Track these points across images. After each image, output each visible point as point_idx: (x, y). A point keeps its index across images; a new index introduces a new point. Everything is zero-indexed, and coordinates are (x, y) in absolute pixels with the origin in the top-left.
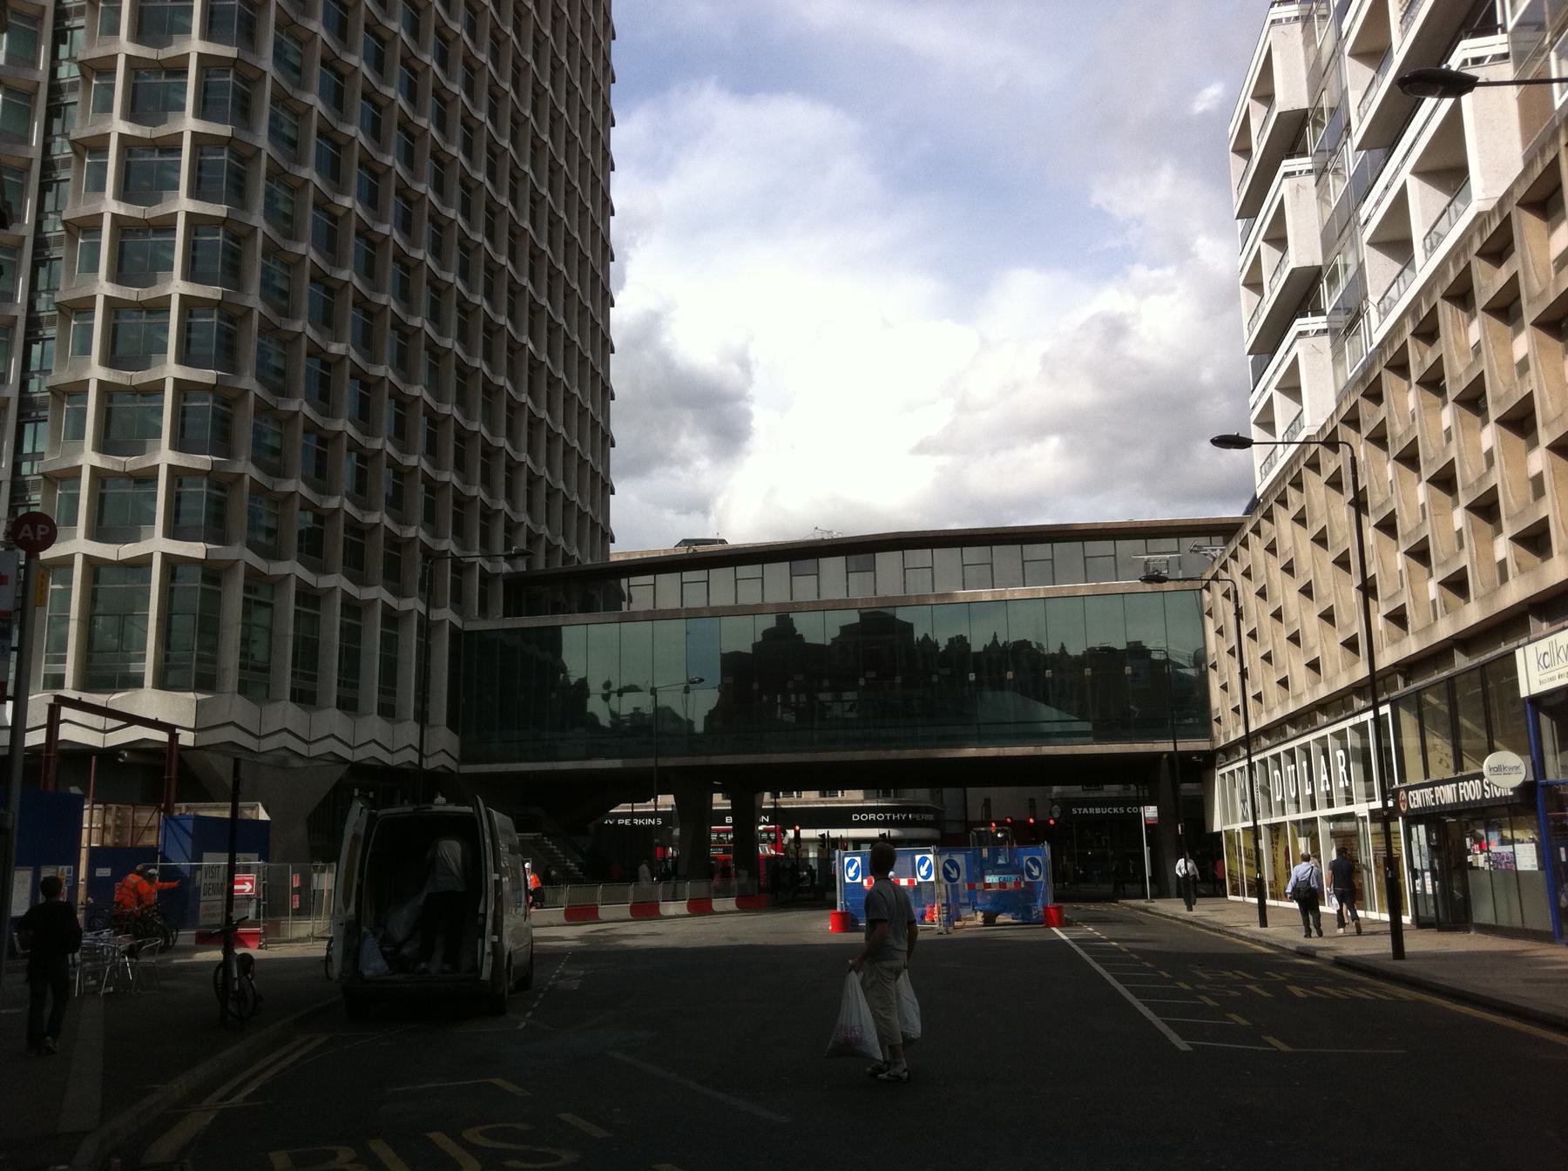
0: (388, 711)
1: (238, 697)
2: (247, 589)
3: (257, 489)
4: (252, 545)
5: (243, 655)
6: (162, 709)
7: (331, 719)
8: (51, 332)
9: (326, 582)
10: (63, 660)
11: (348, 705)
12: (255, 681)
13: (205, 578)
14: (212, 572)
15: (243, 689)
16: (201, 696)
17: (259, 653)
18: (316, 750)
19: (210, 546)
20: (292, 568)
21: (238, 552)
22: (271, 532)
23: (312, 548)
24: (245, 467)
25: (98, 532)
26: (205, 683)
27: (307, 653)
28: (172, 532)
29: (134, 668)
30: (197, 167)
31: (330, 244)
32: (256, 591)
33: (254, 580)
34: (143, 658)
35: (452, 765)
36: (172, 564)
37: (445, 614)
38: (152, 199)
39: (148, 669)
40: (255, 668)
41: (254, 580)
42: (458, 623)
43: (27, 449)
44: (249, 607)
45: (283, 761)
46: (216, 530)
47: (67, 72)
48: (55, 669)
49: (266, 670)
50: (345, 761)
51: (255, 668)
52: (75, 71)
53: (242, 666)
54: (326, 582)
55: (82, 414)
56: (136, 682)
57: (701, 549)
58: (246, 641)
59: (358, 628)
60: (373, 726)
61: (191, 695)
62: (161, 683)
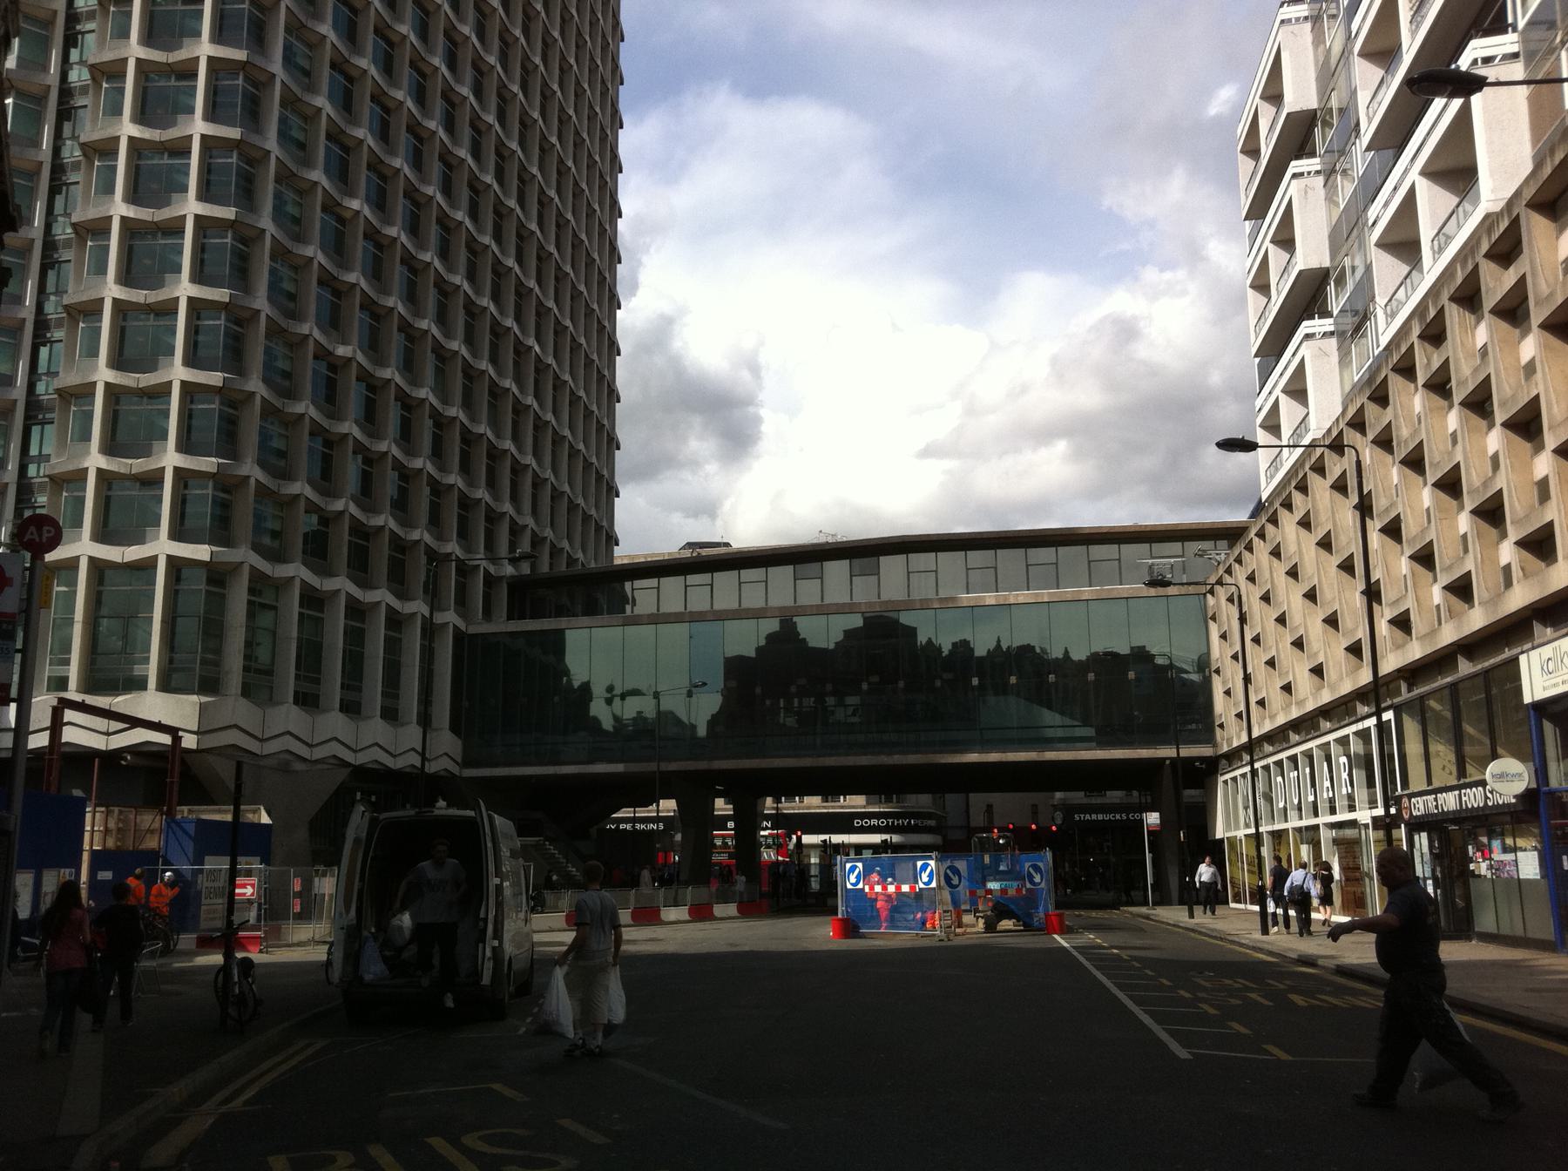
0: (391, 714)
1: (243, 701)
2: (251, 591)
3: (262, 490)
4: (257, 548)
5: (247, 657)
6: (165, 711)
7: (334, 723)
8: (58, 334)
9: (330, 584)
10: (67, 662)
11: (351, 708)
12: (258, 684)
13: (210, 581)
14: (217, 575)
15: (246, 691)
16: (205, 699)
17: (263, 654)
18: (319, 753)
19: (215, 549)
20: (296, 570)
21: (244, 555)
22: (275, 535)
23: (317, 551)
24: (250, 469)
25: (103, 534)
26: (209, 685)
27: (310, 657)
28: (177, 534)
29: (138, 670)
30: (206, 170)
31: (338, 247)
32: (260, 593)
33: (259, 582)
34: (147, 660)
35: (455, 770)
36: (175, 563)
37: (449, 617)
38: (160, 202)
39: (152, 671)
40: (258, 671)
41: (259, 582)
42: (462, 625)
43: (34, 451)
44: (253, 609)
45: (285, 765)
46: (221, 533)
47: (78, 76)
48: (59, 671)
49: (269, 672)
50: (344, 764)
51: (258, 671)
52: (86, 75)
53: (246, 669)
54: (330, 584)
55: (89, 416)
56: (141, 685)
57: (705, 552)
58: (249, 644)
59: (363, 631)
60: (375, 729)
61: (195, 698)
62: (165, 686)
